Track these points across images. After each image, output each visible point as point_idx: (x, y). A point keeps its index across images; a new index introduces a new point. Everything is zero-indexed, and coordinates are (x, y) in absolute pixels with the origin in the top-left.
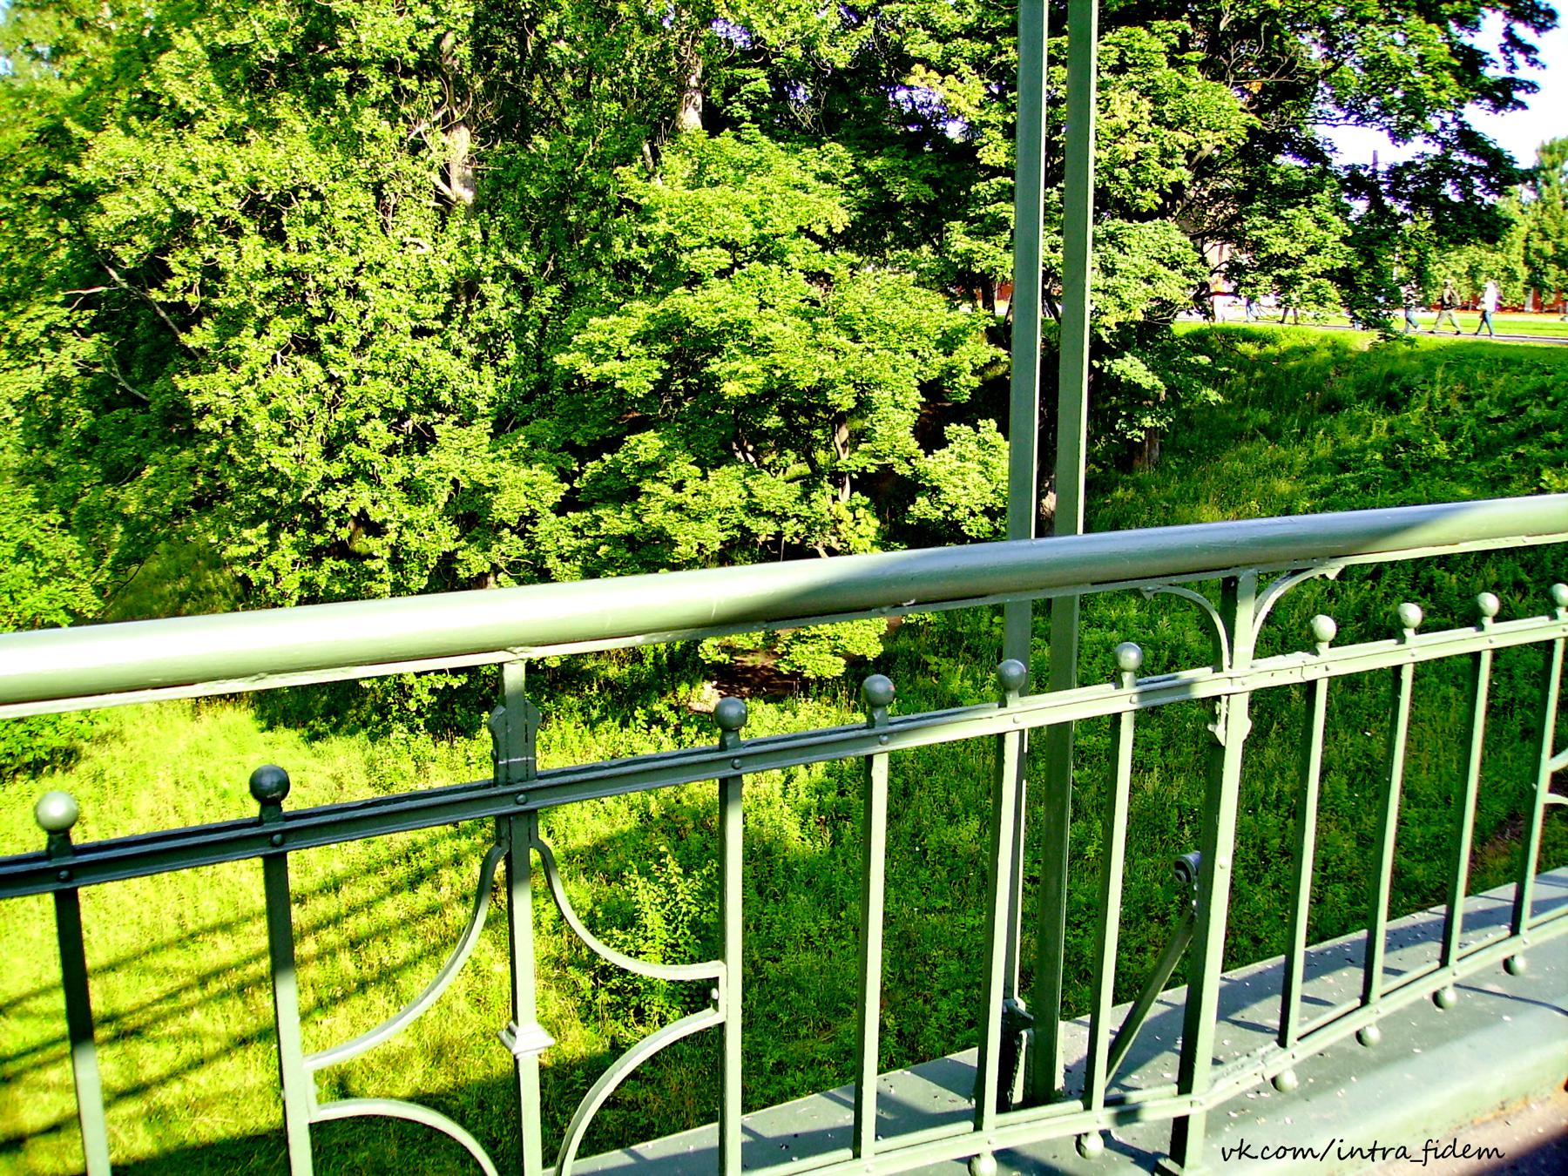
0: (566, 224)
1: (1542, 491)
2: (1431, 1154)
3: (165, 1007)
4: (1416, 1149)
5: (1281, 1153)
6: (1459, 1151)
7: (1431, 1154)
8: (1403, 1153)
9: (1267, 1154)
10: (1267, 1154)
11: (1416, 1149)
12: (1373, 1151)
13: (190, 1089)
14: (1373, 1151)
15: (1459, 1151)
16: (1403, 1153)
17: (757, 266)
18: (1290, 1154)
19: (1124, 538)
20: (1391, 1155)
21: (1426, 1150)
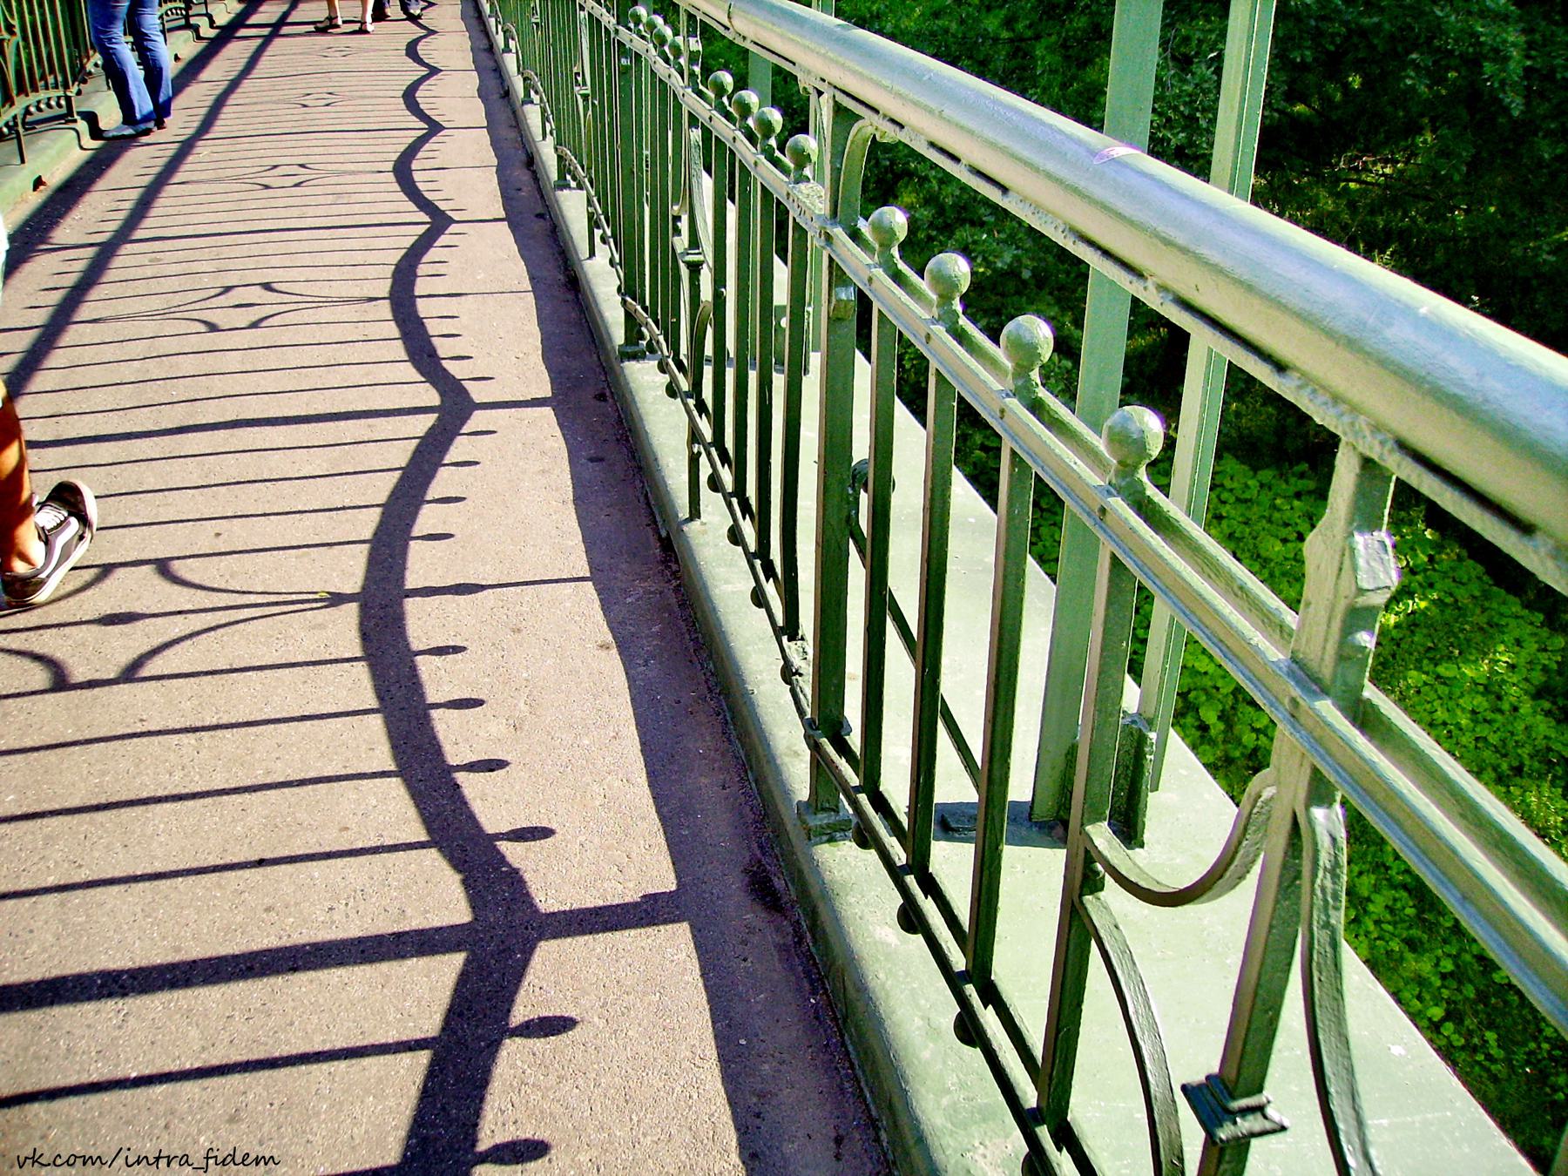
0: (1408, 52)
1: (1218, 457)
2: (211, 1161)
3: (1417, 850)
4: (197, 1158)
5: (71, 1161)
6: (238, 1159)
7: (211, 1161)
8: (185, 1160)
9: (59, 1161)
10: (59, 1161)
11: (197, 1158)
12: (158, 1159)
13: (25, 176)
14: (158, 1159)
15: (238, 1159)
16: (185, 1160)
17: (1015, 298)
18: (80, 1161)
19: (1432, 326)
20: (174, 1165)
21: (207, 1158)
